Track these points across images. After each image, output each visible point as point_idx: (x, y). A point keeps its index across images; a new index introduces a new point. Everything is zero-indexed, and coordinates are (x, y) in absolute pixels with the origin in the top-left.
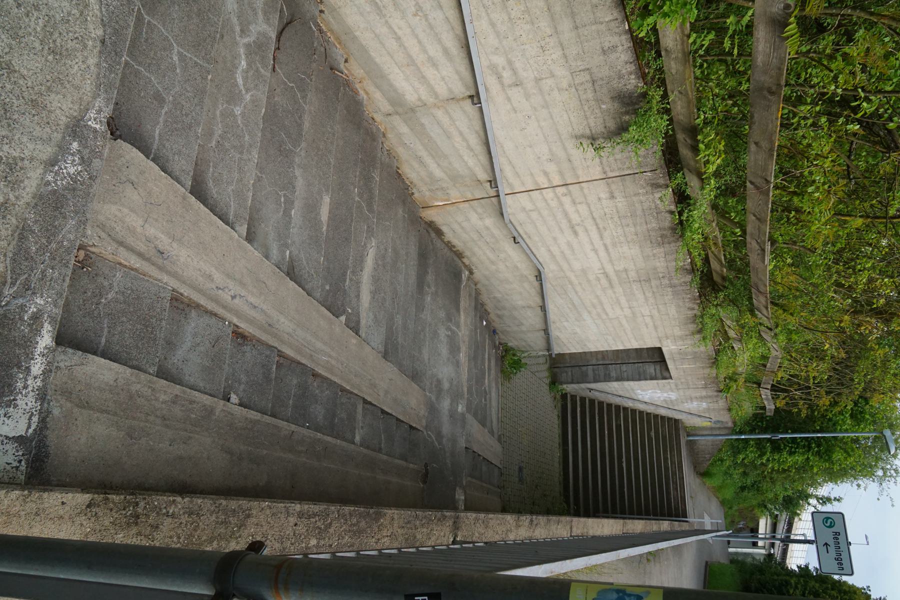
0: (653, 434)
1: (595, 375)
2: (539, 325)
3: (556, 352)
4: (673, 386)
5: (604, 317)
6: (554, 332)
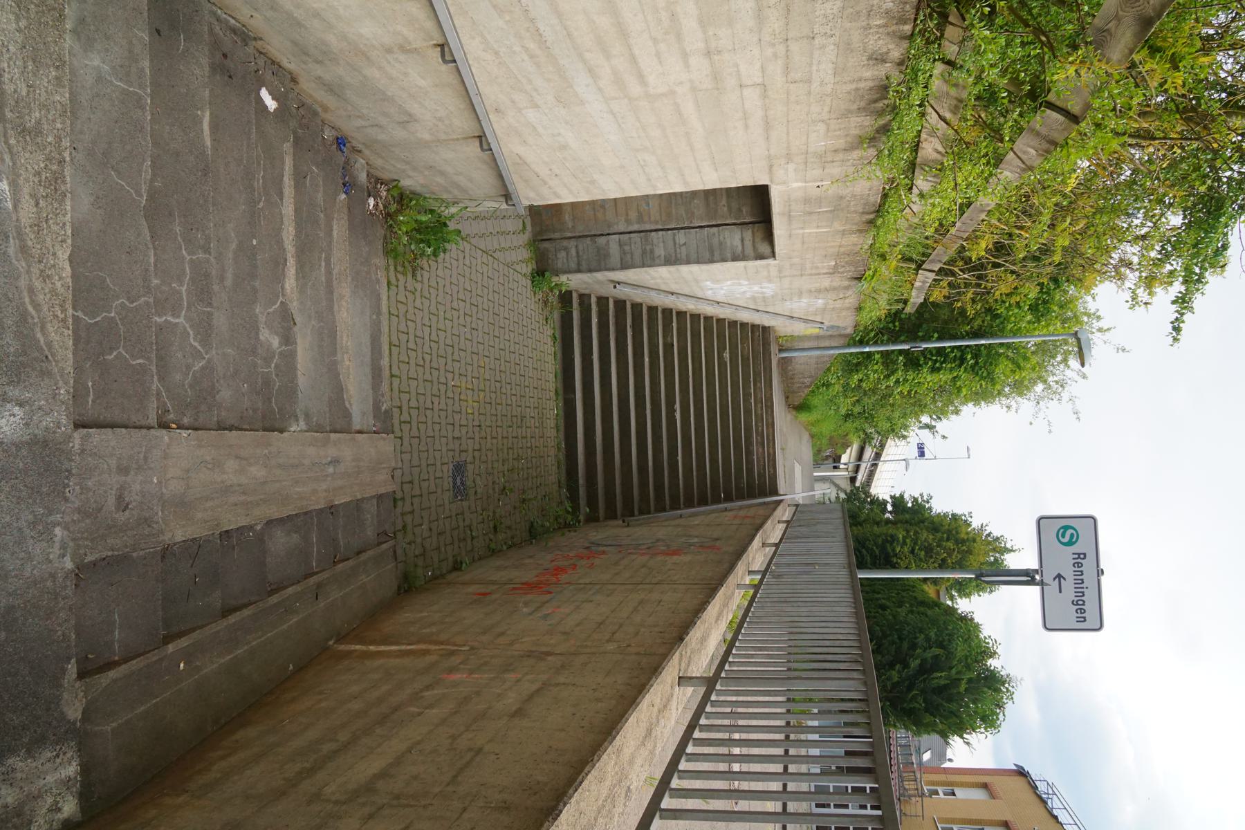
0: (727, 355)
1: (623, 253)
2: (462, 123)
3: (526, 203)
4: (774, 272)
5: (635, 89)
6: (509, 147)
